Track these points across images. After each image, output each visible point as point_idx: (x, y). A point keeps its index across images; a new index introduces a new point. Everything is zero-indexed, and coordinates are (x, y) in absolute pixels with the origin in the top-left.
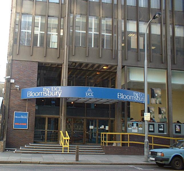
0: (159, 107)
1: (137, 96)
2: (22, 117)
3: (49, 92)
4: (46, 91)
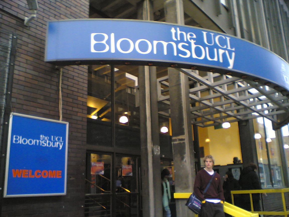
0: (186, 160)
1: (46, 140)
2: (44, 141)
3: (193, 46)
4: (182, 40)
